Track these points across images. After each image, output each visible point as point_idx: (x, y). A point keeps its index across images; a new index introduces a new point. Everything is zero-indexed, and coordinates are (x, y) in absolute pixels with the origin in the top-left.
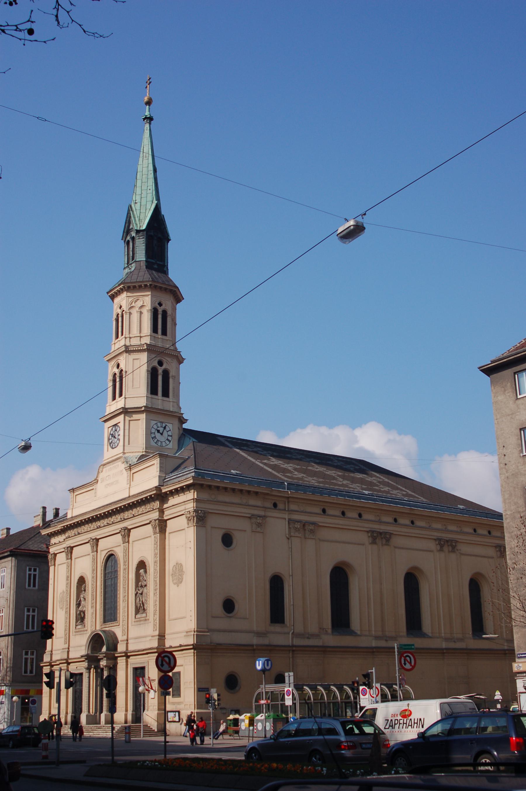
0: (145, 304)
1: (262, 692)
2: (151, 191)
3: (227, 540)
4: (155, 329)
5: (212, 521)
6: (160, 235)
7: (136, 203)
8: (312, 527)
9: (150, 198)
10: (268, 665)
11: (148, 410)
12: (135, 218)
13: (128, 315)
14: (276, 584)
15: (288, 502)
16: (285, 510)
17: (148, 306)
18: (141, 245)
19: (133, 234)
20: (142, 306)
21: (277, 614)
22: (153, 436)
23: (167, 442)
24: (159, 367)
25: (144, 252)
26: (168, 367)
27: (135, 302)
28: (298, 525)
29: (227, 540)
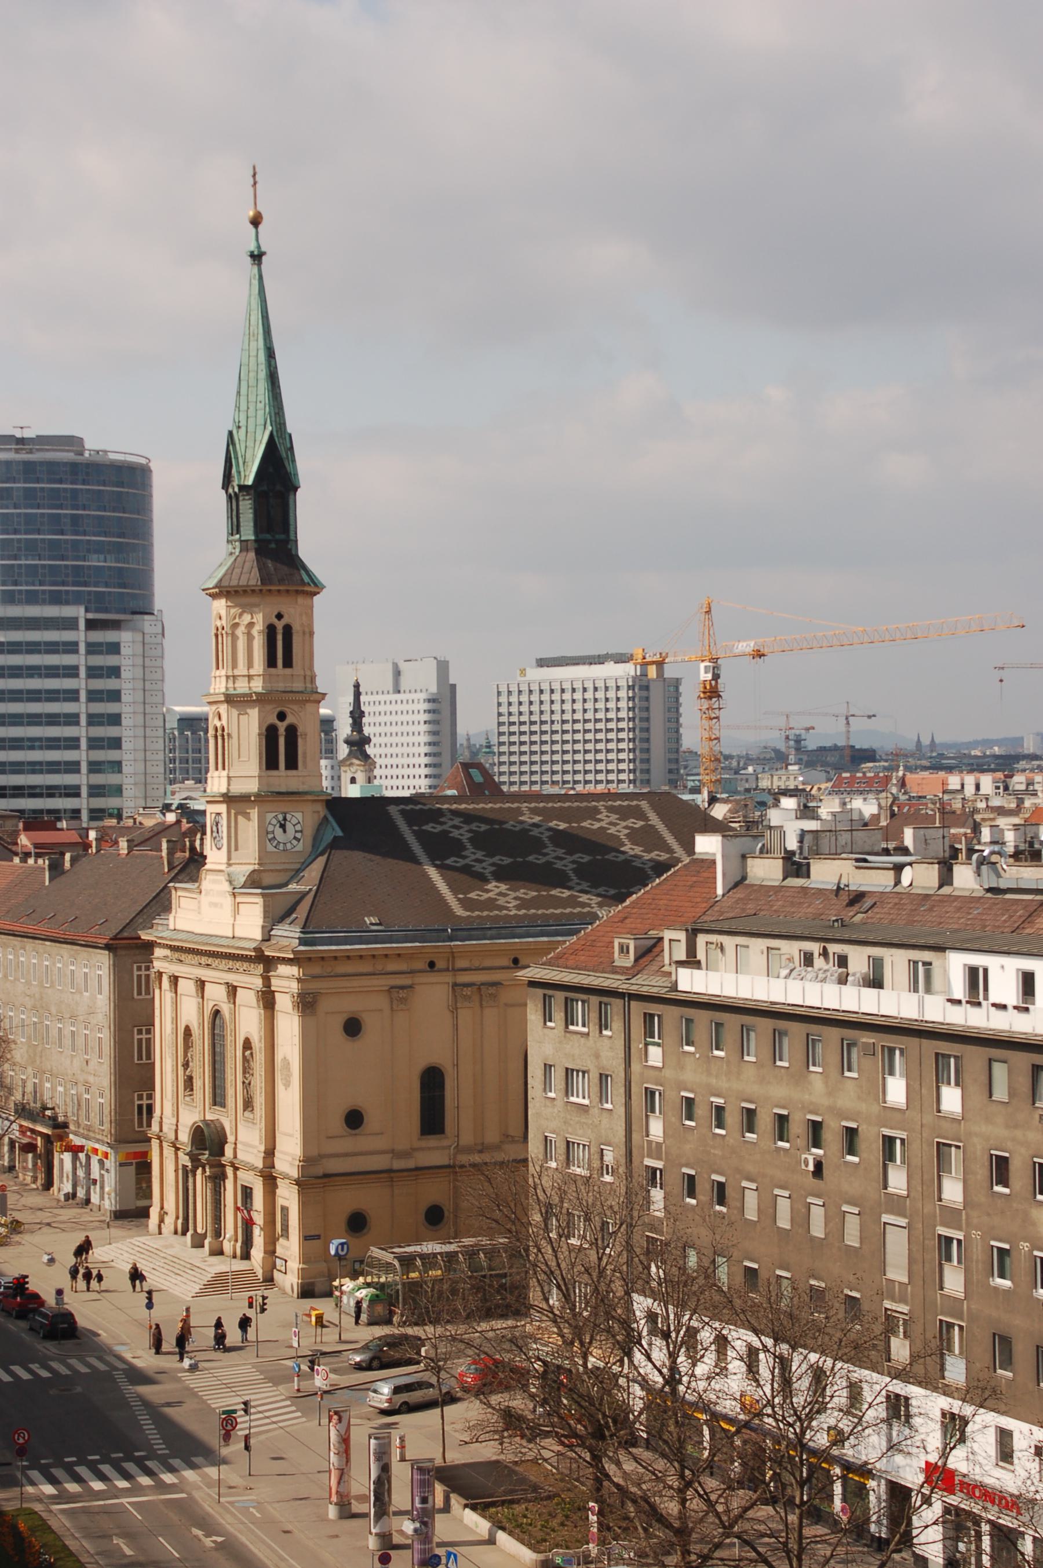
0: (254, 620)
2: (262, 405)
3: (353, 1027)
4: (271, 662)
5: (325, 1005)
6: (278, 487)
8: (492, 990)
10: (342, 1250)
11: (263, 798)
13: (230, 638)
14: (432, 1081)
15: (453, 957)
16: (447, 970)
17: (259, 627)
20: (251, 625)
21: (432, 1119)
22: (270, 836)
23: (295, 842)
24: (279, 723)
25: (252, 524)
28: (467, 991)
29: (353, 1027)
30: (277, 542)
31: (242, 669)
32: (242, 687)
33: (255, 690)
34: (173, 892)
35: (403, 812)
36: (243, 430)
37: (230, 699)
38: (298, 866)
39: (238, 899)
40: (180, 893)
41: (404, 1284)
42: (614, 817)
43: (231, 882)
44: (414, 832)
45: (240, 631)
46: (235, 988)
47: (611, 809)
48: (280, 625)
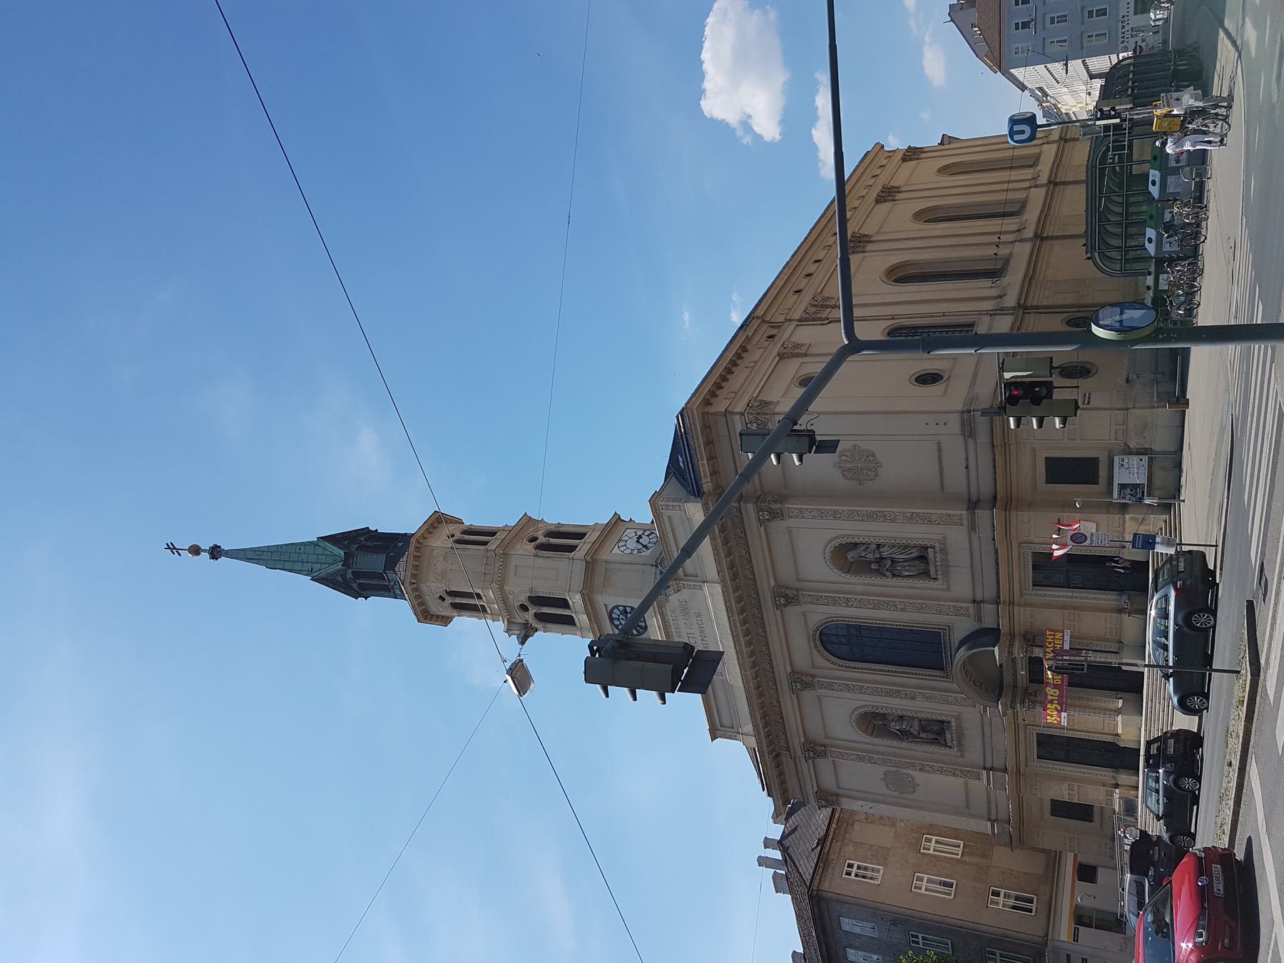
19: (349, 575)
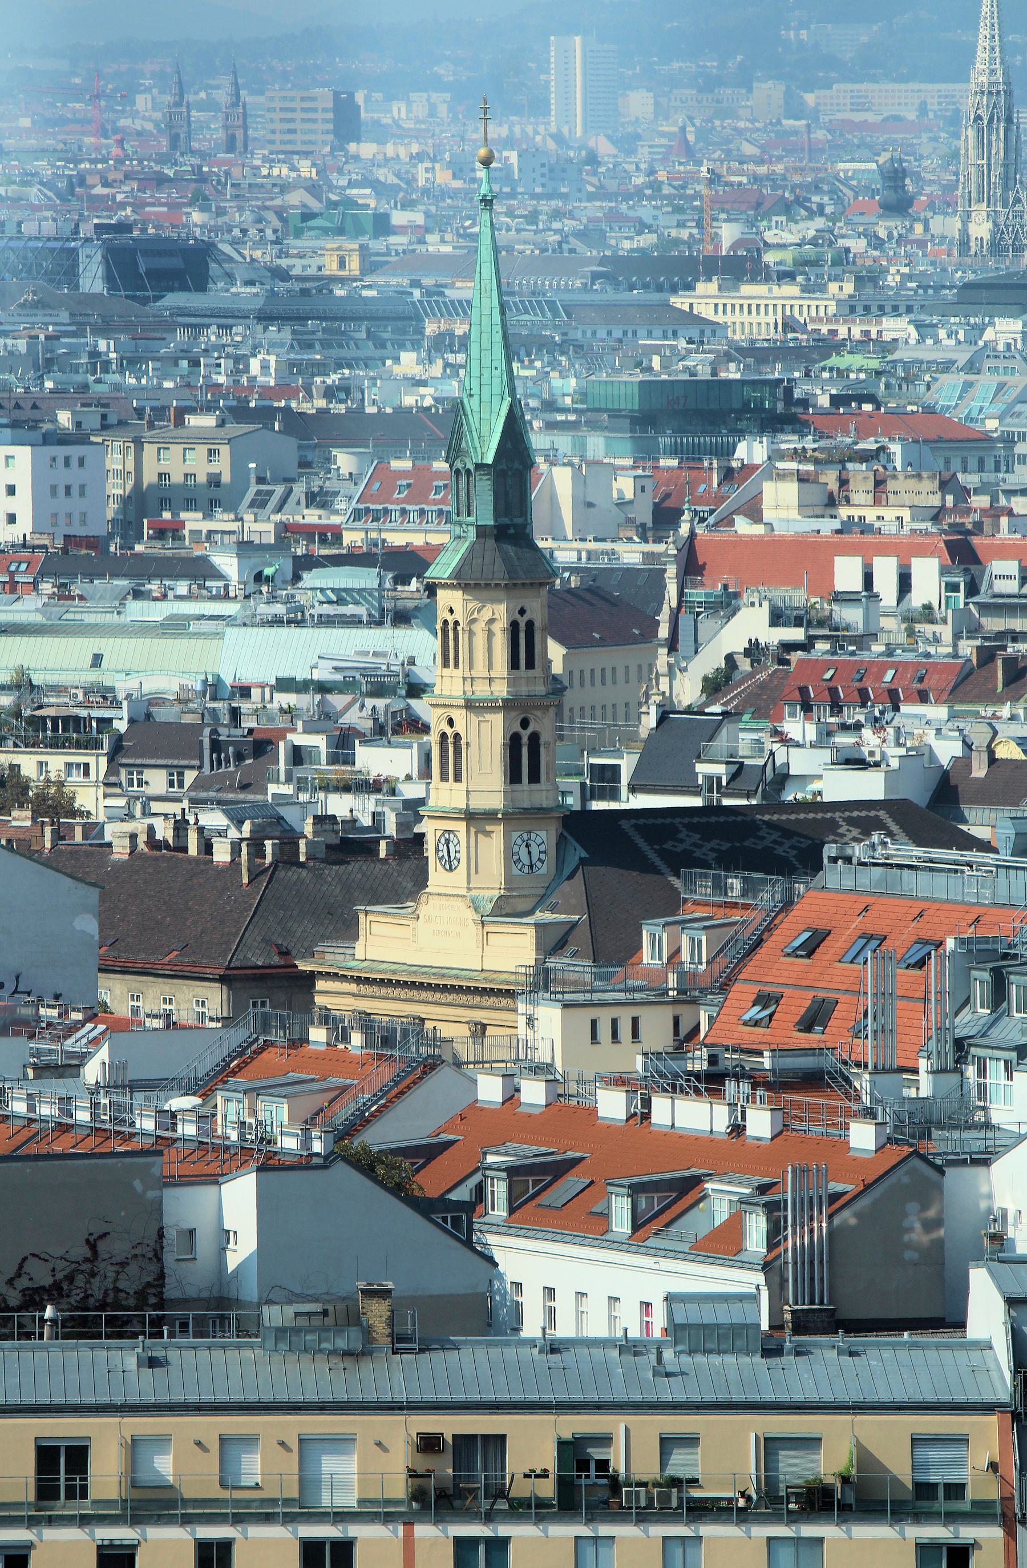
0: (497, 616)
1: (786, 1201)
4: (514, 664)
6: (517, 465)
7: (471, 395)
9: (497, 389)
12: (471, 432)
13: (467, 635)
17: (501, 626)
18: (484, 490)
20: (492, 621)
22: (516, 858)
25: (491, 508)
26: (538, 729)
27: (479, 611)
30: (515, 526)
31: (480, 669)
32: (482, 691)
33: (496, 694)
34: (362, 916)
35: (636, 827)
36: (476, 398)
37: (470, 705)
38: (541, 892)
39: (487, 929)
40: (370, 918)
41: (676, 1343)
42: (698, 854)
43: (477, 910)
44: (656, 851)
45: (479, 628)
46: (484, 1026)
47: (851, 822)
48: (522, 622)
